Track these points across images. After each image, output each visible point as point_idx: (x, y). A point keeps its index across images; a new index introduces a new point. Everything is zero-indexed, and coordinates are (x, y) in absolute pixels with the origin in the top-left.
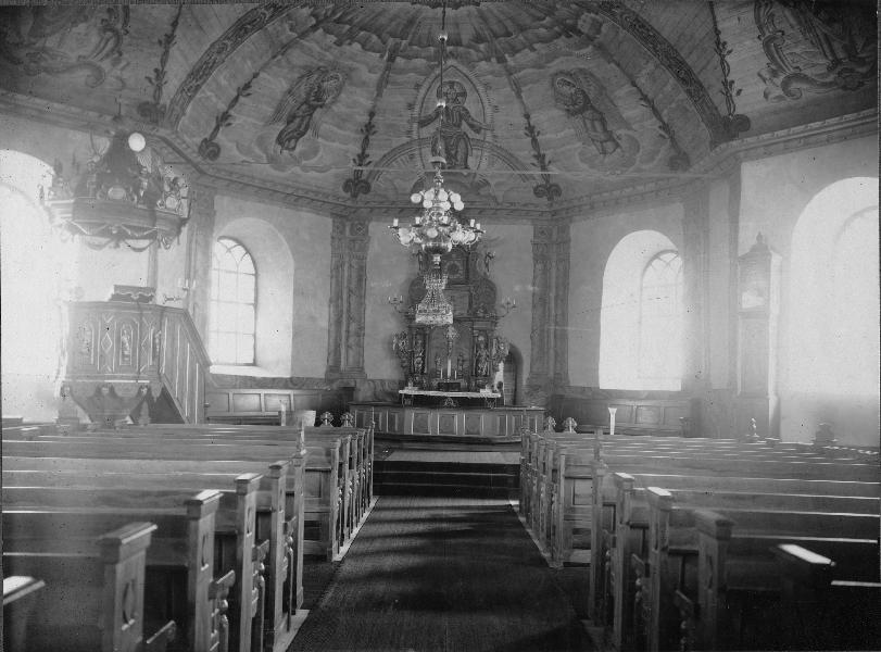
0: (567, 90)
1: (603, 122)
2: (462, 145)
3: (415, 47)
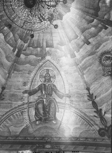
3: (31, 48)
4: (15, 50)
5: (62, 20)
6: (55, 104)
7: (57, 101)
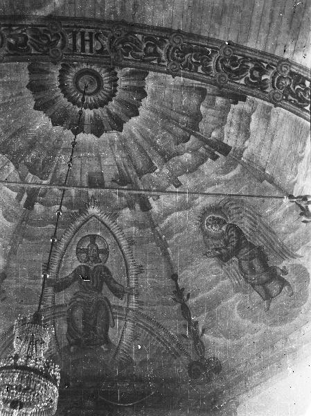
0: (213, 230)
1: (264, 260)
2: (102, 313)
4: (22, 198)
5: (121, 131)
6: (106, 309)
7: (112, 303)
